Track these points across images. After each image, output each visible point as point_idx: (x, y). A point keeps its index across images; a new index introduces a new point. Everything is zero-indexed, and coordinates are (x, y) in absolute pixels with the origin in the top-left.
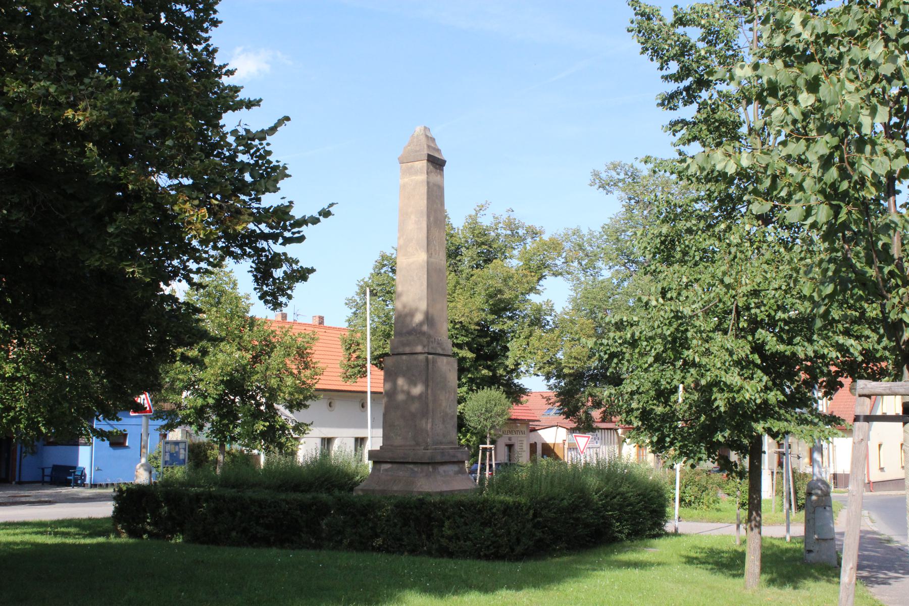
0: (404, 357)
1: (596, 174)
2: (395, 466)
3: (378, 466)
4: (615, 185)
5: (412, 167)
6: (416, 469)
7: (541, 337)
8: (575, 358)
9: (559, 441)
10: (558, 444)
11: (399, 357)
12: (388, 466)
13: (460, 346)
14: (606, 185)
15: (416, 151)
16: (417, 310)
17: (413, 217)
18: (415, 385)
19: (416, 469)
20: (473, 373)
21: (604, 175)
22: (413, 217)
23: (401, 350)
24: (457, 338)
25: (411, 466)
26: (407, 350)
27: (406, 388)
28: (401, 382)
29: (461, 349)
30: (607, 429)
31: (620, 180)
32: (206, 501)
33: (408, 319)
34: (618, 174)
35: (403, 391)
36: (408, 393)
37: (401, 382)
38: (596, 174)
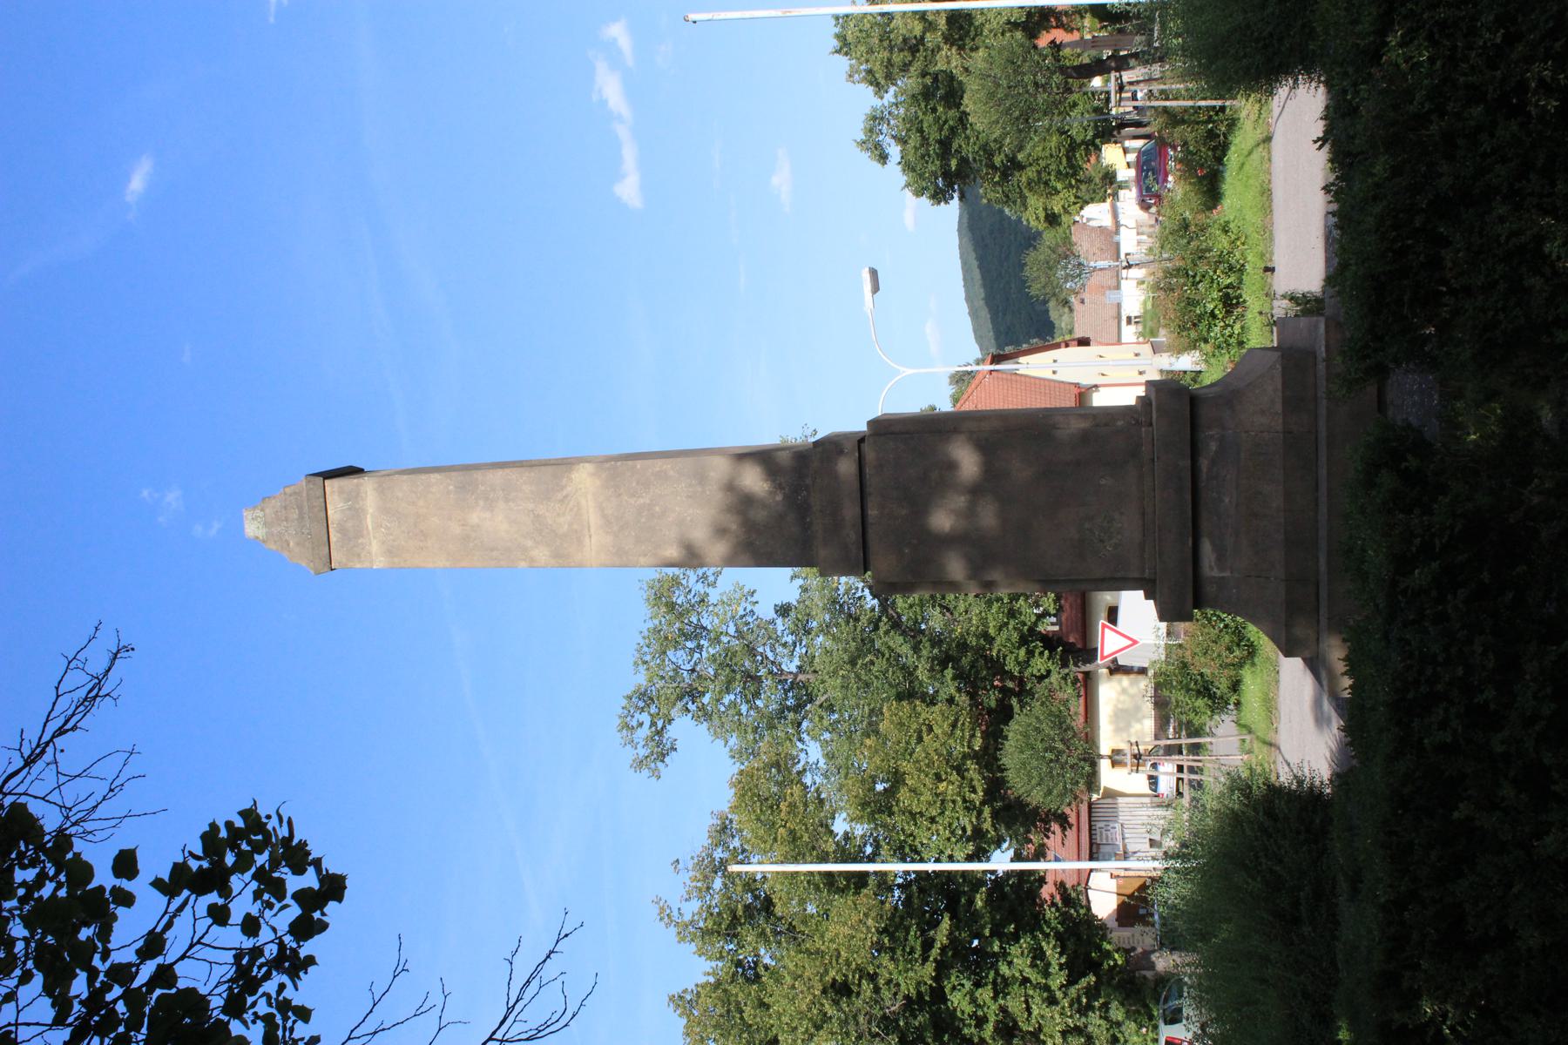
0: (872, 512)
1: (640, 764)
2: (1205, 525)
3: (1210, 590)
4: (659, 733)
5: (342, 530)
6: (1213, 446)
7: (913, 791)
8: (954, 725)
9: (1112, 885)
10: (1119, 887)
11: (871, 532)
12: (1207, 548)
13: (928, 945)
14: (660, 750)
15: (301, 517)
16: (730, 487)
17: (474, 517)
18: (952, 466)
19: (1213, 446)
20: (983, 927)
21: (643, 752)
22: (474, 517)
23: (852, 535)
24: (912, 951)
25: (1204, 464)
26: (850, 512)
27: (960, 501)
28: (942, 520)
29: (933, 940)
30: (1090, 817)
31: (653, 724)
32: (1410, 1001)
33: (760, 515)
34: (641, 725)
35: (970, 513)
36: (976, 491)
37: (942, 520)
38: (640, 764)
